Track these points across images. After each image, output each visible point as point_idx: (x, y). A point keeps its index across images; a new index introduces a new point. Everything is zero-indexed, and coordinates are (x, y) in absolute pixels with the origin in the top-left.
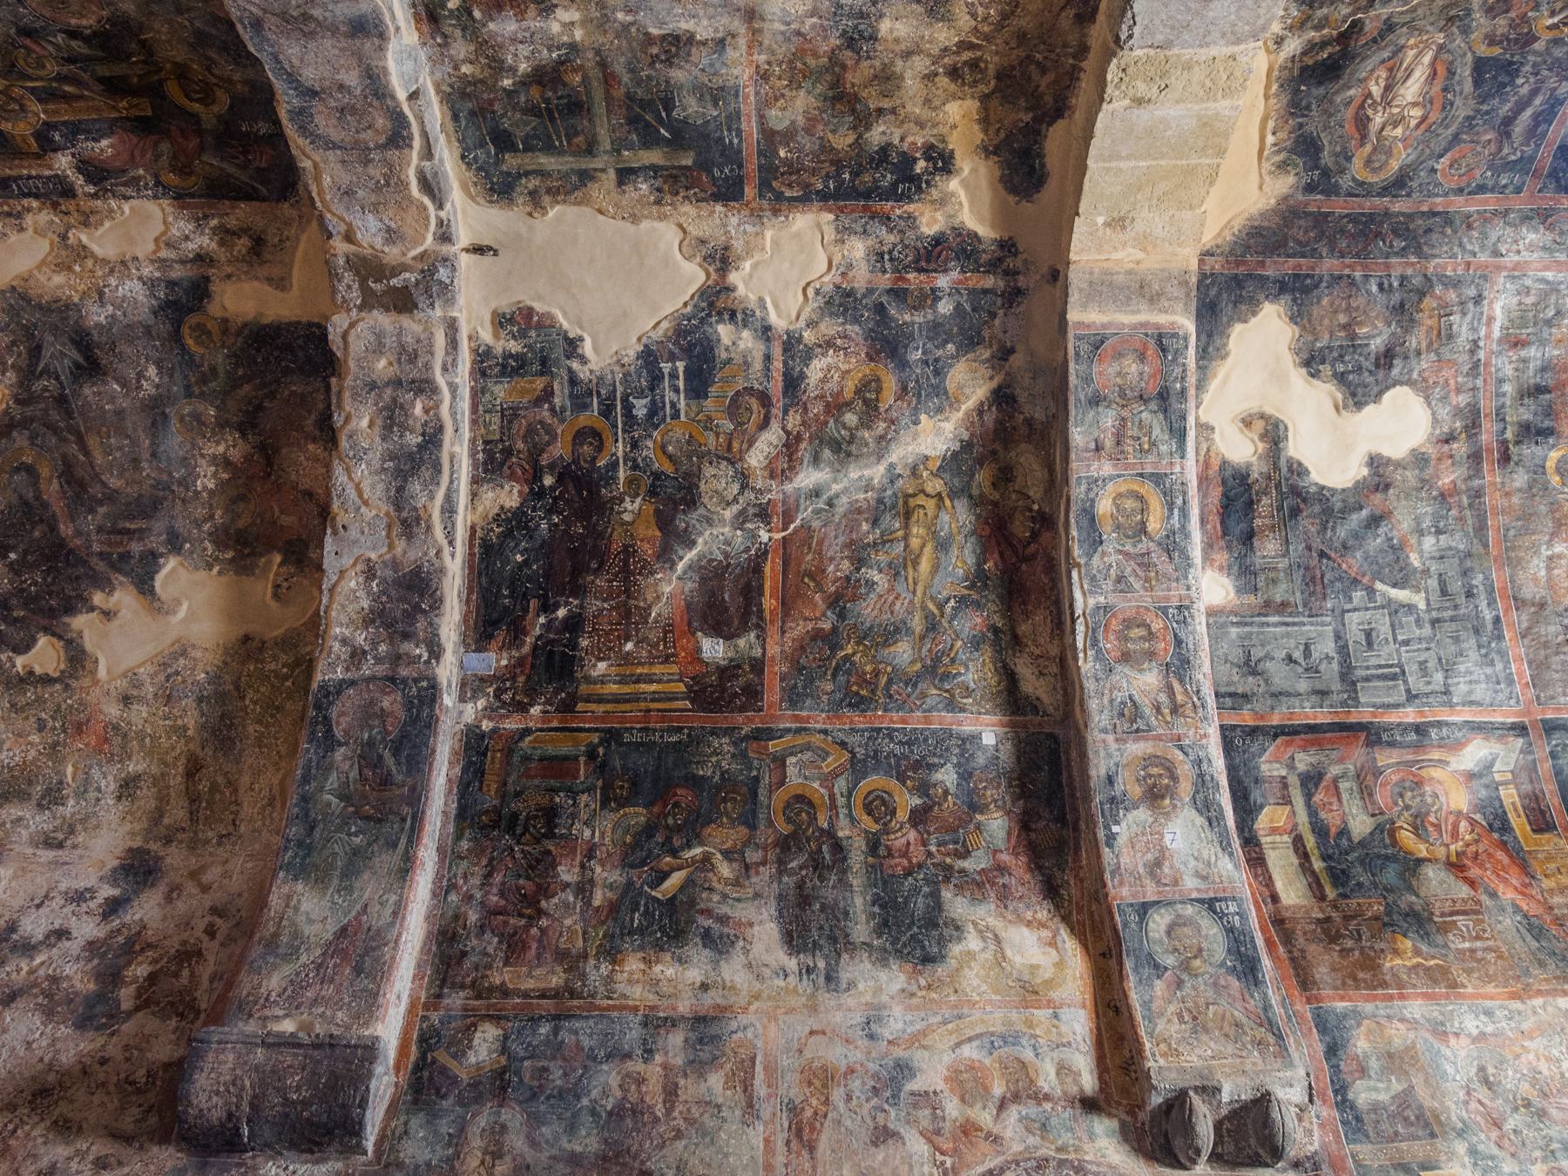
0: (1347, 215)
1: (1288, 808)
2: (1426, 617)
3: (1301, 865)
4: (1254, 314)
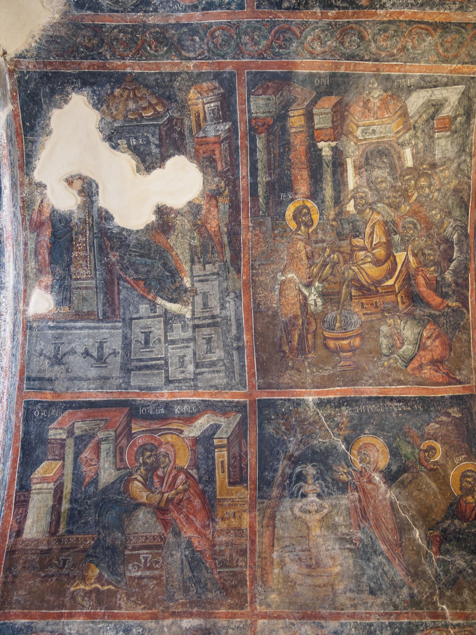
0: (116, 27)
1: (60, 463)
2: (191, 323)
3: (53, 507)
4: (66, 102)
